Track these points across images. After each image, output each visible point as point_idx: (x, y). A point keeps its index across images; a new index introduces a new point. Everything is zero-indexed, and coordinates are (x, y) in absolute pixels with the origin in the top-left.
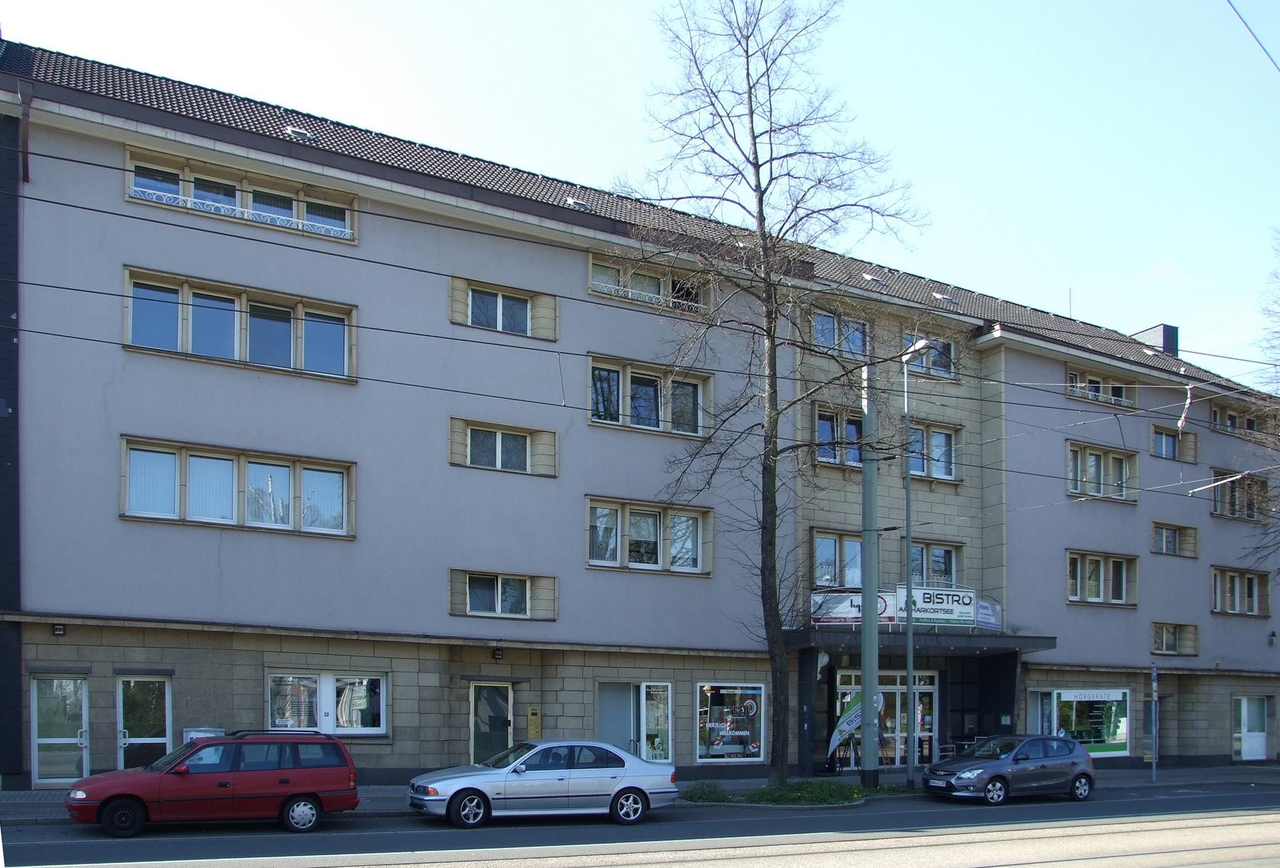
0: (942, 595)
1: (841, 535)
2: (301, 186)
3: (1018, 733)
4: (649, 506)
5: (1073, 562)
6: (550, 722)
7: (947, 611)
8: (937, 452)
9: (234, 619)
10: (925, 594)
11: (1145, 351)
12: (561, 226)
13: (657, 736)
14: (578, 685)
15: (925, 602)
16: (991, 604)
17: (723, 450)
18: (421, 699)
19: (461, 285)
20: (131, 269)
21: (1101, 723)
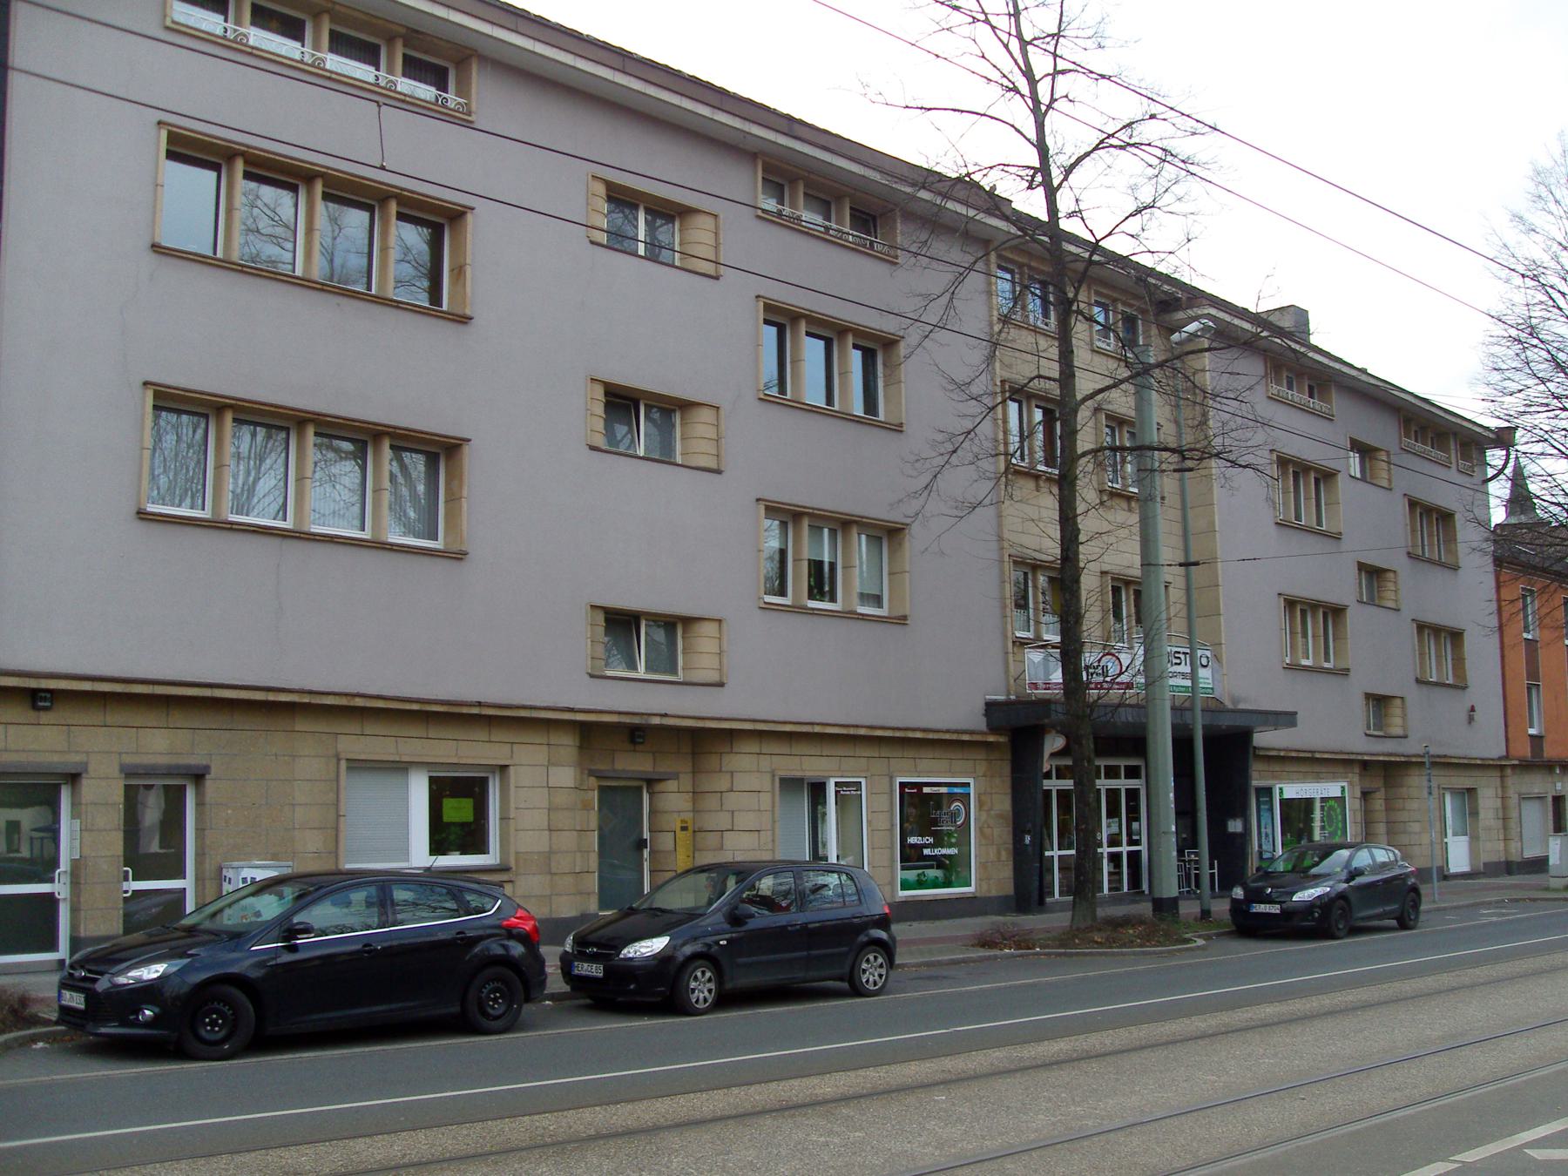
2: (403, 31)
18: (551, 809)
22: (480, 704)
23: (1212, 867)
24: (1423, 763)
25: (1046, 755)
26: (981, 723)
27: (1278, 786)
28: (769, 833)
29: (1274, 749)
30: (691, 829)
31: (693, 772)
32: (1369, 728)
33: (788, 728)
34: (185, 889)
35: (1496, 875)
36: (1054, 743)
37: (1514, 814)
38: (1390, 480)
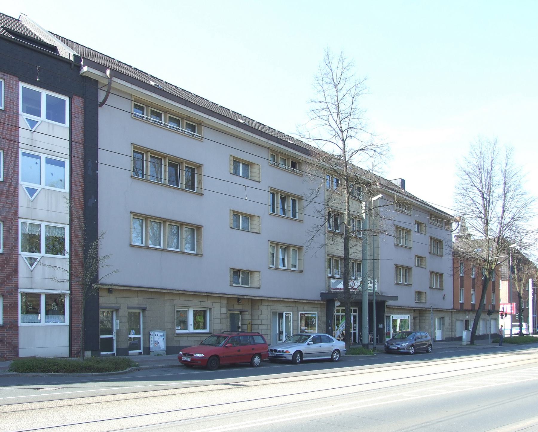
4: (283, 245)
12: (265, 140)
18: (221, 319)
20: (271, 188)
23: (377, 336)
24: (431, 310)
25: (335, 307)
26: (319, 298)
27: (392, 316)
28: (270, 325)
29: (391, 306)
30: (251, 324)
32: (416, 300)
33: (275, 299)
34: (140, 337)
35: (449, 341)
36: (337, 304)
37: (454, 324)
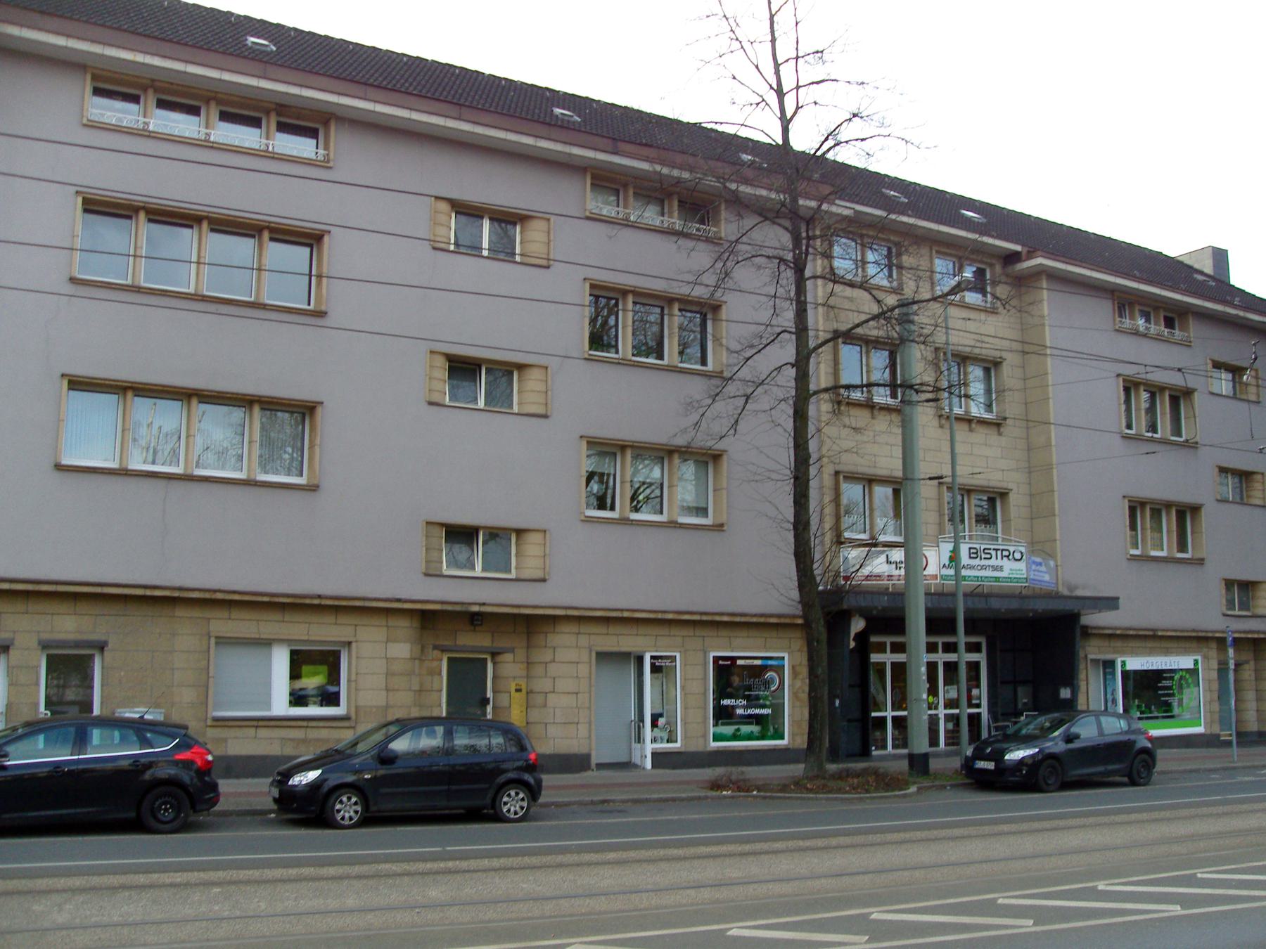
0: (990, 549)
1: (870, 481)
2: (274, 106)
3: (1079, 708)
5: (1132, 510)
6: (539, 699)
7: (996, 568)
8: (977, 388)
9: (177, 582)
10: (970, 548)
11: (1195, 276)
13: (661, 715)
14: (572, 655)
15: (970, 558)
16: (1043, 559)
17: (749, 391)
18: (389, 674)
19: (444, 206)
21: (1173, 695)
22: (319, 597)
29: (1108, 628)
31: (528, 647)
38: (1258, 395)
